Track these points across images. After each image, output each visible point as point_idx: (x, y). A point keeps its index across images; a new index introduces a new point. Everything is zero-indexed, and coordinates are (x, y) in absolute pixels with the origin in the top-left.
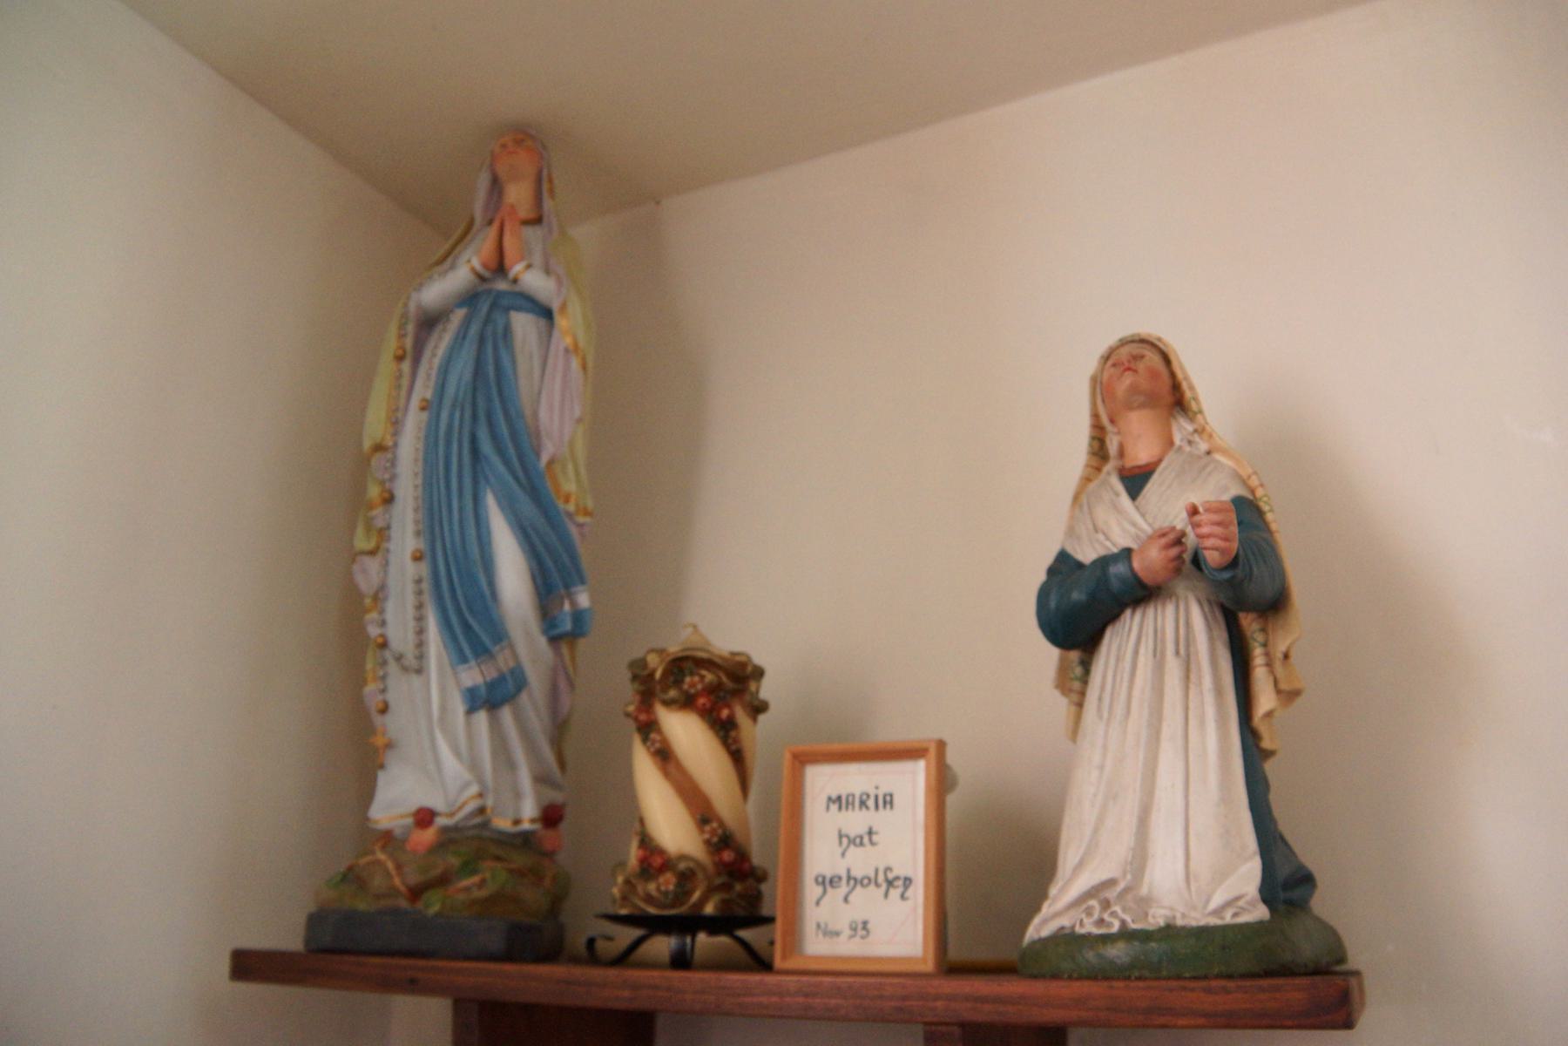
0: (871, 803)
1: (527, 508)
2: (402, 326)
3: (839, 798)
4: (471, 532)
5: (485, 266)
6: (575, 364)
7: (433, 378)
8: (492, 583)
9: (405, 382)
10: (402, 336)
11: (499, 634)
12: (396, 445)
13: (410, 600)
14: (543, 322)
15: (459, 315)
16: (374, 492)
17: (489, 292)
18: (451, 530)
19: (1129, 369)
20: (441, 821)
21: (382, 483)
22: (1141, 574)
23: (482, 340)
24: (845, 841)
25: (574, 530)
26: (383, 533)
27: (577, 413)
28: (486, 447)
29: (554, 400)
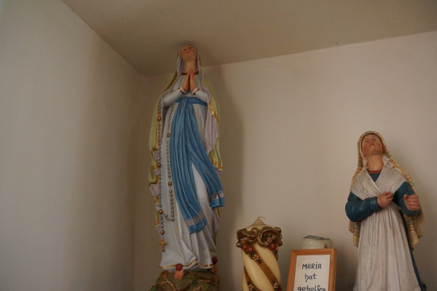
0: (315, 267)
1: (204, 167)
2: (159, 110)
3: (306, 265)
4: (188, 177)
5: (184, 90)
6: (215, 120)
7: (171, 126)
8: (195, 193)
9: (161, 127)
10: (159, 113)
11: (198, 208)
12: (160, 149)
13: (169, 198)
14: (203, 106)
15: (177, 104)
16: (154, 164)
17: (186, 97)
18: (182, 177)
19: (373, 144)
20: (184, 268)
21: (157, 161)
22: (380, 205)
23: (185, 114)
24: (307, 277)
25: (218, 173)
26: (159, 177)
27: (217, 137)
28: (190, 149)
29: (209, 133)
